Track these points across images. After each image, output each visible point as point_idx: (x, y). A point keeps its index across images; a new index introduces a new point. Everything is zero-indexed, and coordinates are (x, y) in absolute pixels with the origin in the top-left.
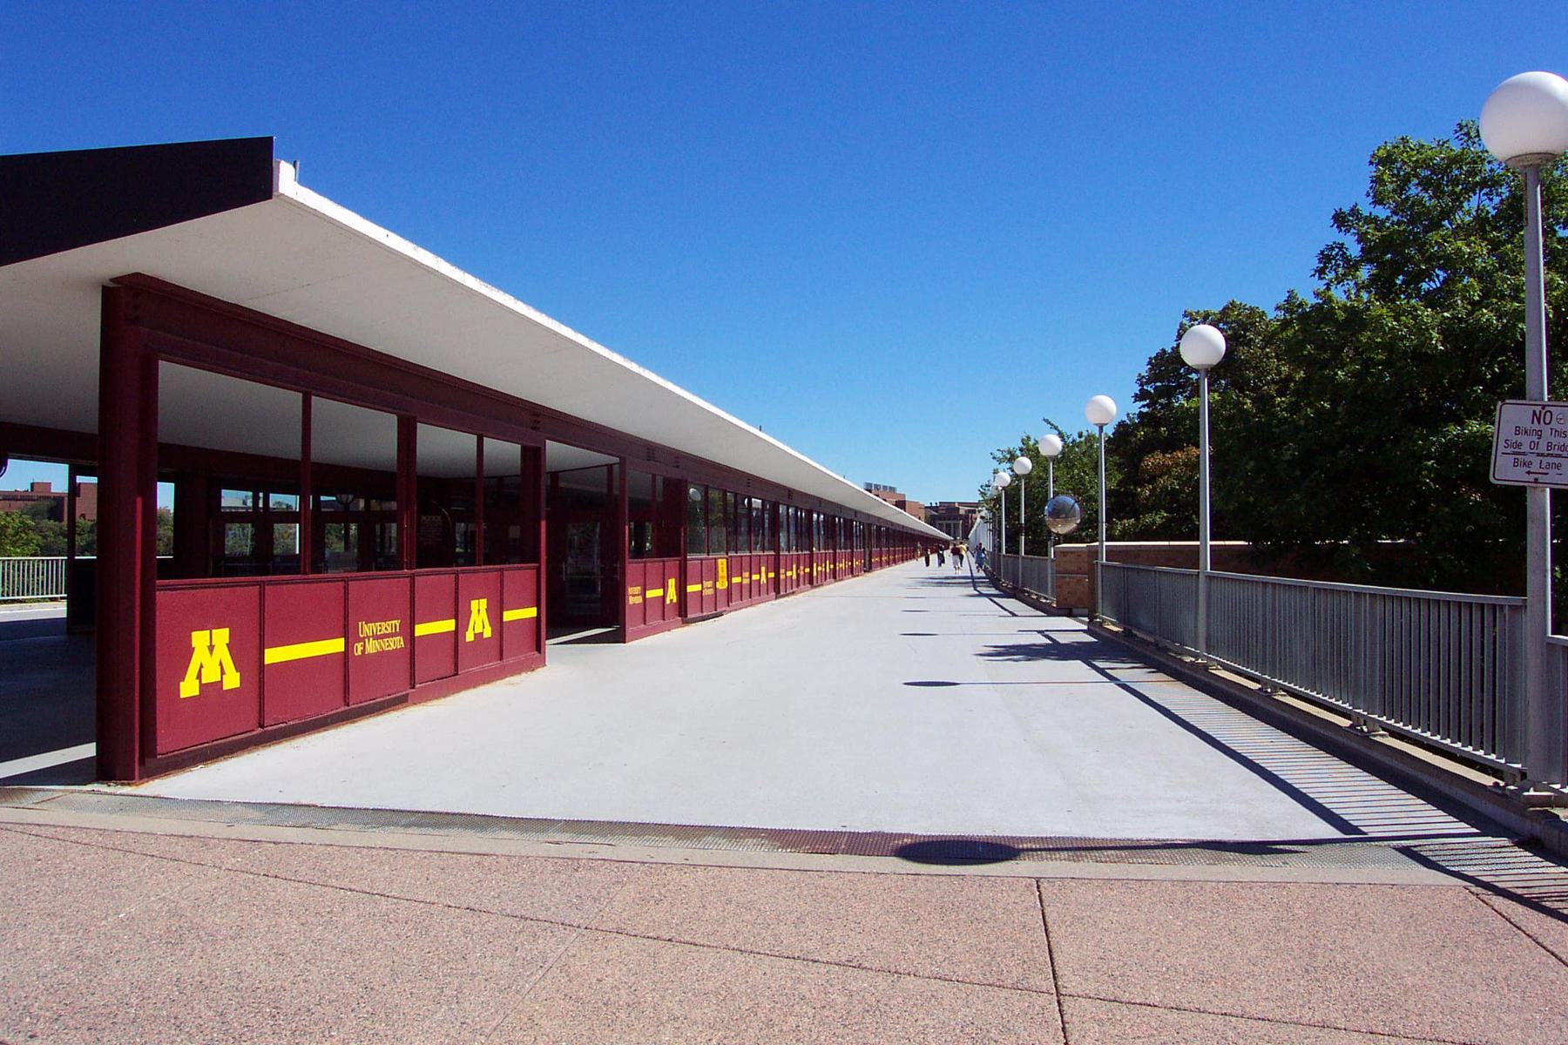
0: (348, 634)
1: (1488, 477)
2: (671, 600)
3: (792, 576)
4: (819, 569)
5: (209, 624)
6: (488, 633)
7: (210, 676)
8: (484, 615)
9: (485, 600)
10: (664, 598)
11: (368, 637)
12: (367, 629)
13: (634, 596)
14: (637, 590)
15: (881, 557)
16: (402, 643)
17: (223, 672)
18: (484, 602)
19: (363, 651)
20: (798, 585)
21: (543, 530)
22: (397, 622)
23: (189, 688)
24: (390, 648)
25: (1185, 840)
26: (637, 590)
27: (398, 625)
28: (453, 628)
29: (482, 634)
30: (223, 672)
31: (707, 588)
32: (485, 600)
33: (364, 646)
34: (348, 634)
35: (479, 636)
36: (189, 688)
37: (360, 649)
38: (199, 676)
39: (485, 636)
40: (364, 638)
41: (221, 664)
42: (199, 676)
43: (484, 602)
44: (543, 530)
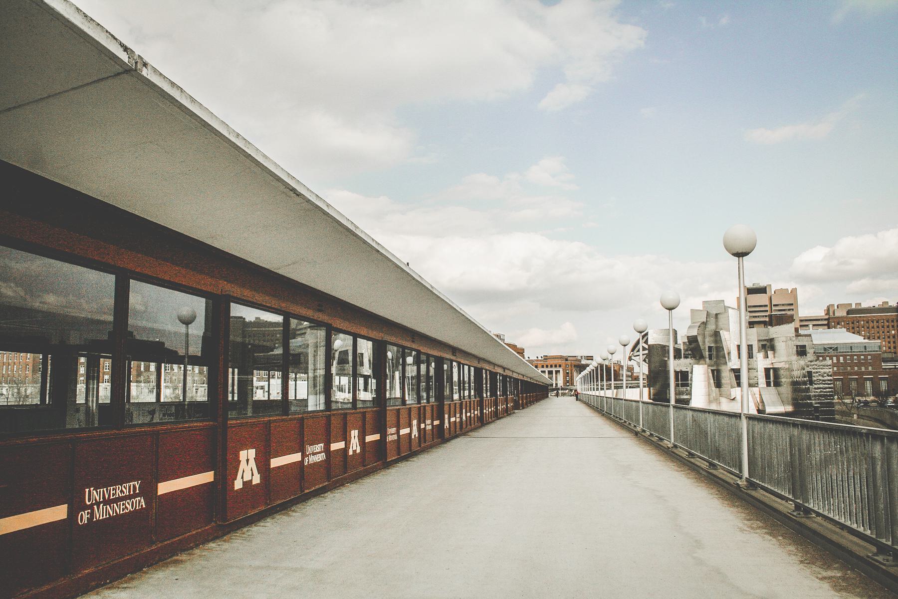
0: (303, 451)
1: (85, 502)
2: (354, 451)
3: (477, 414)
4: (453, 419)
5: (355, 429)
6: (257, 480)
7: (247, 477)
8: (252, 463)
9: (357, 431)
10: (410, 434)
11: (98, 504)
12: (94, 494)
13: (392, 434)
14: (393, 430)
15: (496, 405)
16: (325, 457)
17: (253, 475)
18: (252, 453)
19: (308, 462)
20: (750, 312)
21: (47, 399)
22: (322, 445)
23: (238, 485)
24: (319, 460)
25: (543, 383)
26: (393, 430)
27: (137, 487)
28: (343, 446)
29: (356, 450)
30: (253, 475)
31: (392, 434)
32: (357, 431)
33: (308, 459)
34: (303, 451)
35: (248, 484)
36: (238, 485)
37: (307, 461)
38: (242, 478)
39: (254, 483)
40: (92, 505)
41: (252, 470)
42: (242, 478)
43: (252, 453)
44: (47, 399)
